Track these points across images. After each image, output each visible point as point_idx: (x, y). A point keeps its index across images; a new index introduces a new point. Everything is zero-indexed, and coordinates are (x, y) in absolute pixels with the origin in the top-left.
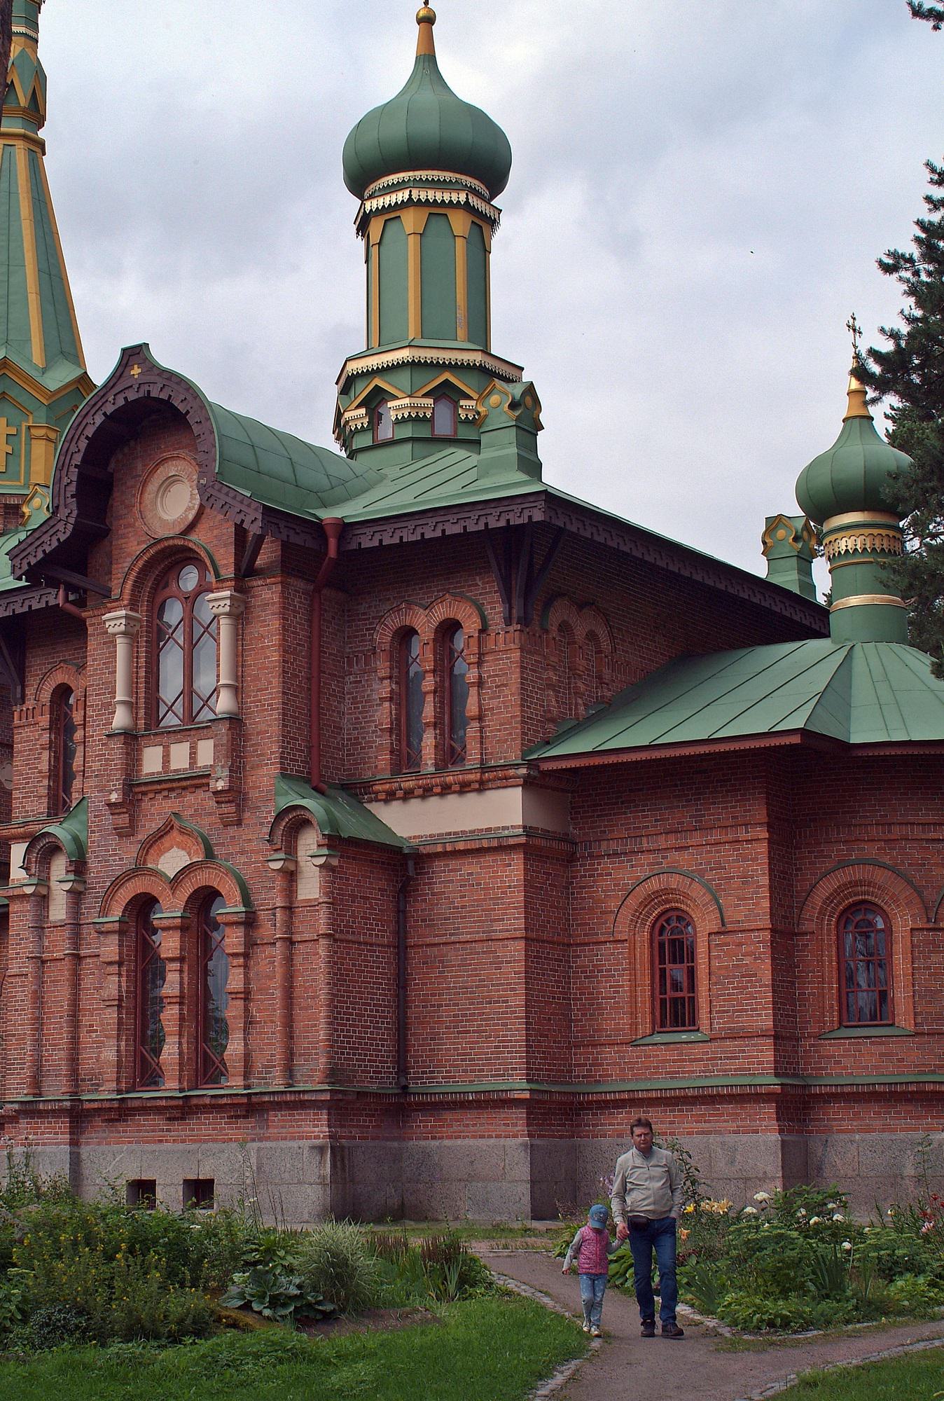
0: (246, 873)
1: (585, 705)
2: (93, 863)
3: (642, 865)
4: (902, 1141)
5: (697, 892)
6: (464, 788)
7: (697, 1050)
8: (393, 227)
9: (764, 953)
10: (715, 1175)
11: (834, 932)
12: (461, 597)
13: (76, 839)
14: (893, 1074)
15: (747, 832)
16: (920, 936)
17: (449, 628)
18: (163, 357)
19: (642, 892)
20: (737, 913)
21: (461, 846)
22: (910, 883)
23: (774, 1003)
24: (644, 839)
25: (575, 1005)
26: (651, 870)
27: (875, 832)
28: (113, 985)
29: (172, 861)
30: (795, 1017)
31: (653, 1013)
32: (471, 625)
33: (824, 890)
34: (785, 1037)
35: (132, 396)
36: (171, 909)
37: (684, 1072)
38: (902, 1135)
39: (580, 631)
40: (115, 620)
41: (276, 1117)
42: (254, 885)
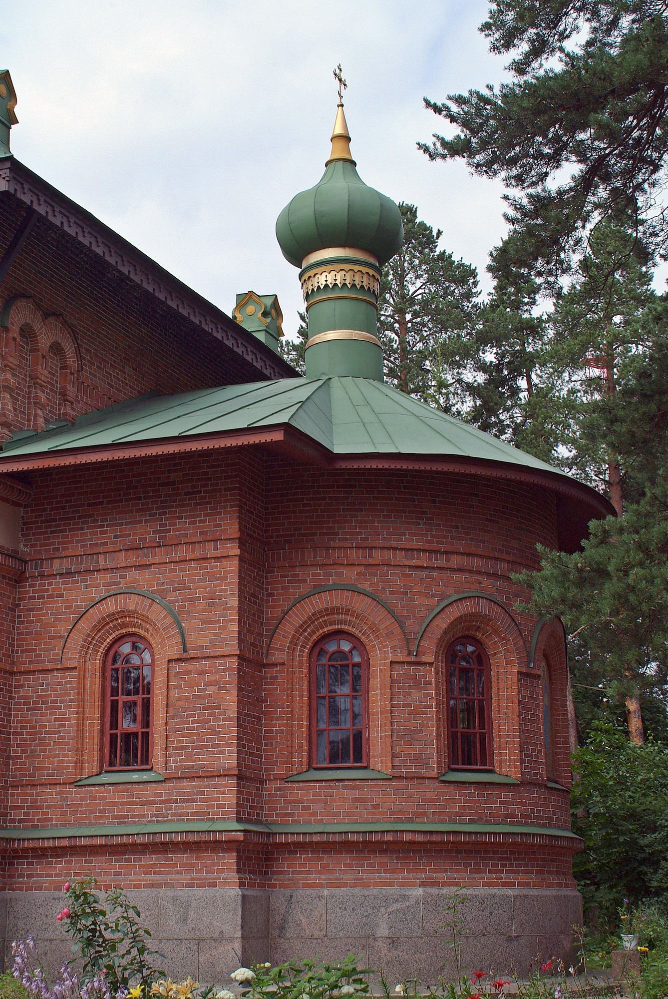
1: (45, 419)
3: (98, 586)
4: (376, 897)
5: (157, 614)
7: (149, 792)
9: (229, 682)
10: (164, 935)
11: (306, 664)
14: (366, 822)
15: (216, 549)
16: (401, 670)
19: (96, 614)
20: (199, 639)
22: (390, 612)
23: (239, 738)
24: (102, 557)
25: (15, 740)
26: (107, 591)
27: (354, 555)
30: (260, 757)
31: (101, 750)
33: (296, 619)
34: (249, 778)
37: (133, 816)
38: (375, 891)
39: (45, 340)
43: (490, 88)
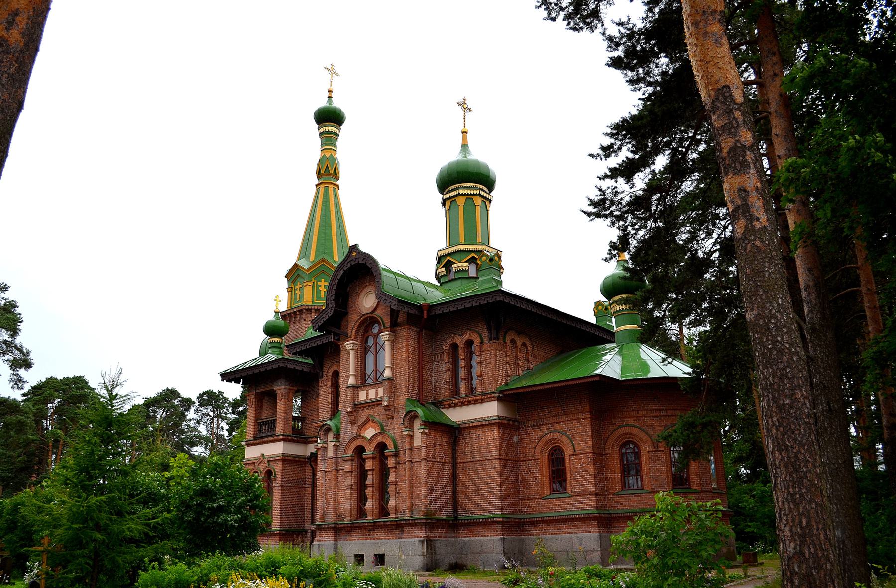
0: (396, 436)
2: (342, 434)
5: (565, 439)
6: (476, 402)
7: (567, 501)
8: (454, 204)
12: (473, 331)
13: (336, 426)
17: (470, 343)
18: (363, 248)
20: (580, 447)
21: (475, 424)
22: (647, 434)
28: (349, 480)
29: (369, 433)
32: (477, 341)
35: (353, 263)
36: (370, 450)
39: (519, 343)
40: (349, 345)
41: (406, 530)
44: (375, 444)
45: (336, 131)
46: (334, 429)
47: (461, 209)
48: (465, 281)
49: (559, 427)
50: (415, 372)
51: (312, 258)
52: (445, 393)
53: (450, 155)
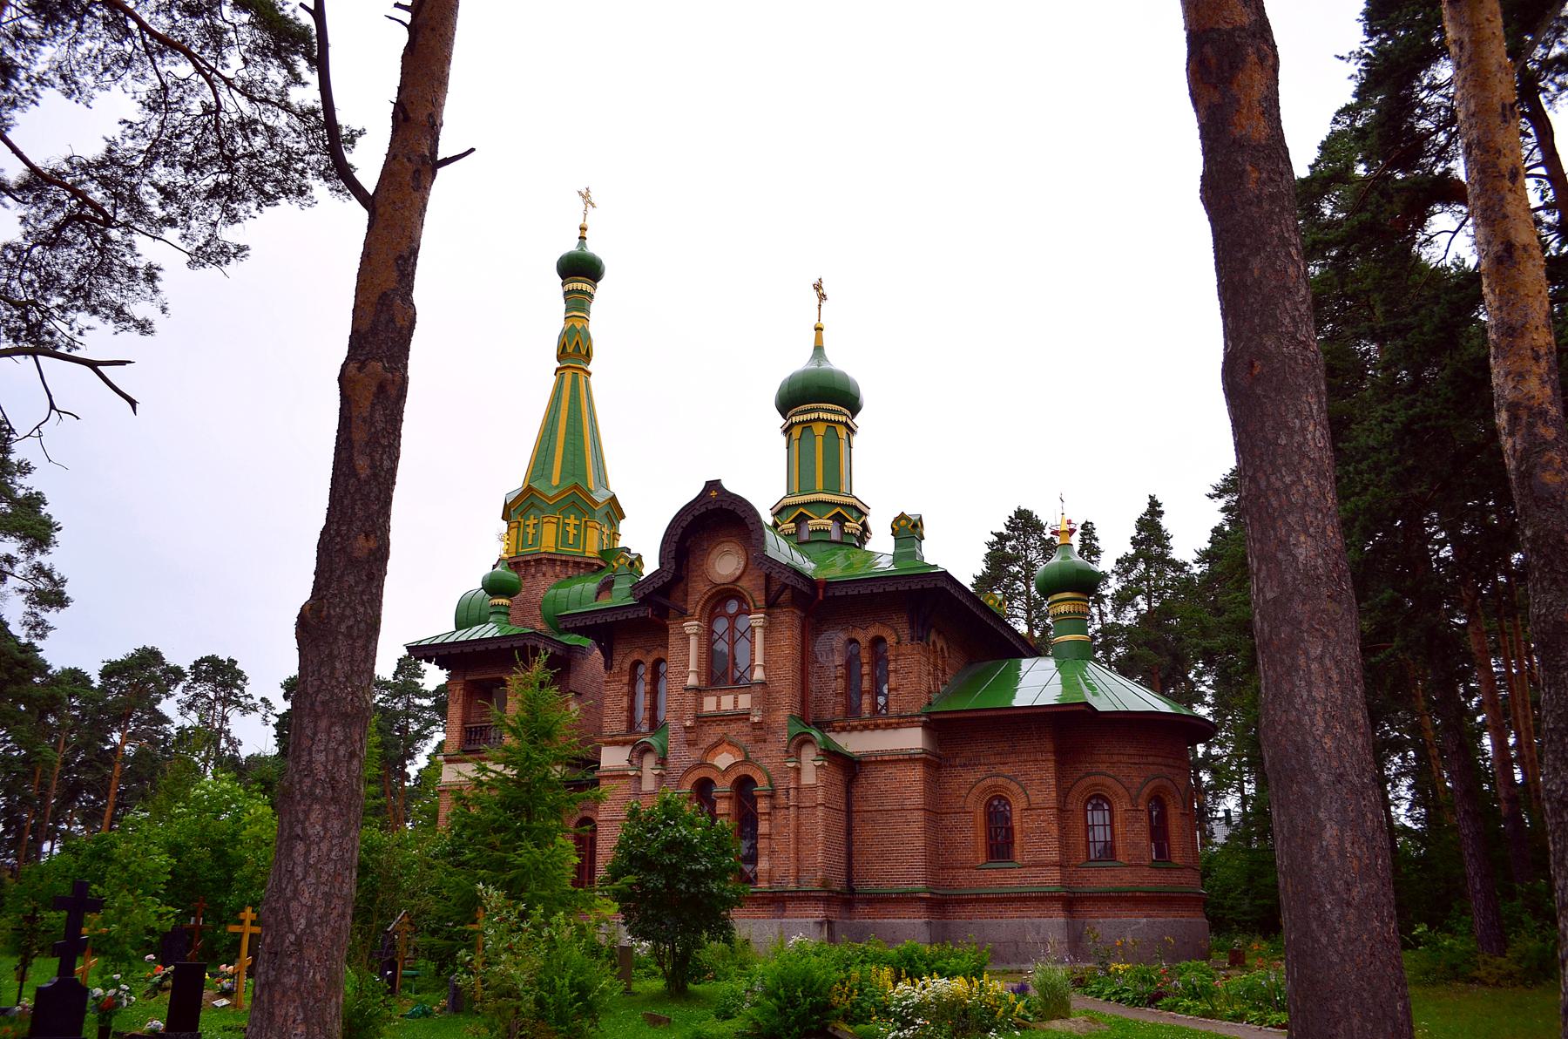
0: (770, 768)
2: (670, 758)
5: (1014, 786)
6: (888, 726)
7: (1014, 872)
8: (807, 432)
17: (878, 641)
18: (730, 486)
20: (1036, 799)
29: (723, 760)
32: (891, 640)
35: (711, 507)
36: (723, 786)
41: (790, 906)
42: (775, 775)
43: (212, 254)
44: (733, 776)
45: (589, 288)
46: (658, 749)
47: (819, 440)
48: (825, 547)
49: (1005, 769)
50: (798, 676)
51: (555, 480)
52: (833, 708)
53: (797, 361)
